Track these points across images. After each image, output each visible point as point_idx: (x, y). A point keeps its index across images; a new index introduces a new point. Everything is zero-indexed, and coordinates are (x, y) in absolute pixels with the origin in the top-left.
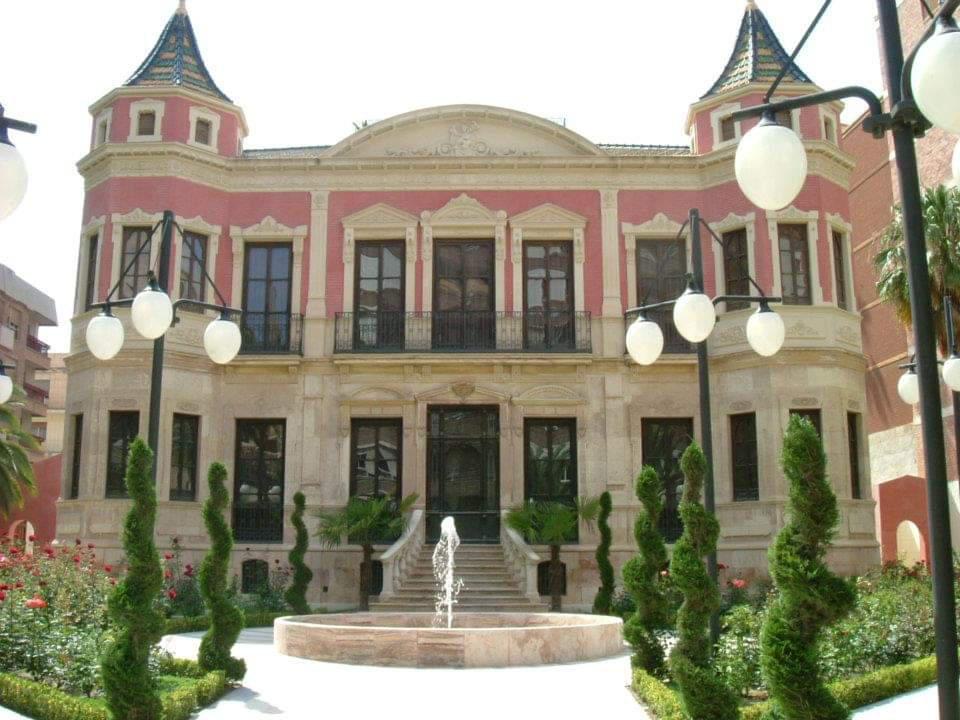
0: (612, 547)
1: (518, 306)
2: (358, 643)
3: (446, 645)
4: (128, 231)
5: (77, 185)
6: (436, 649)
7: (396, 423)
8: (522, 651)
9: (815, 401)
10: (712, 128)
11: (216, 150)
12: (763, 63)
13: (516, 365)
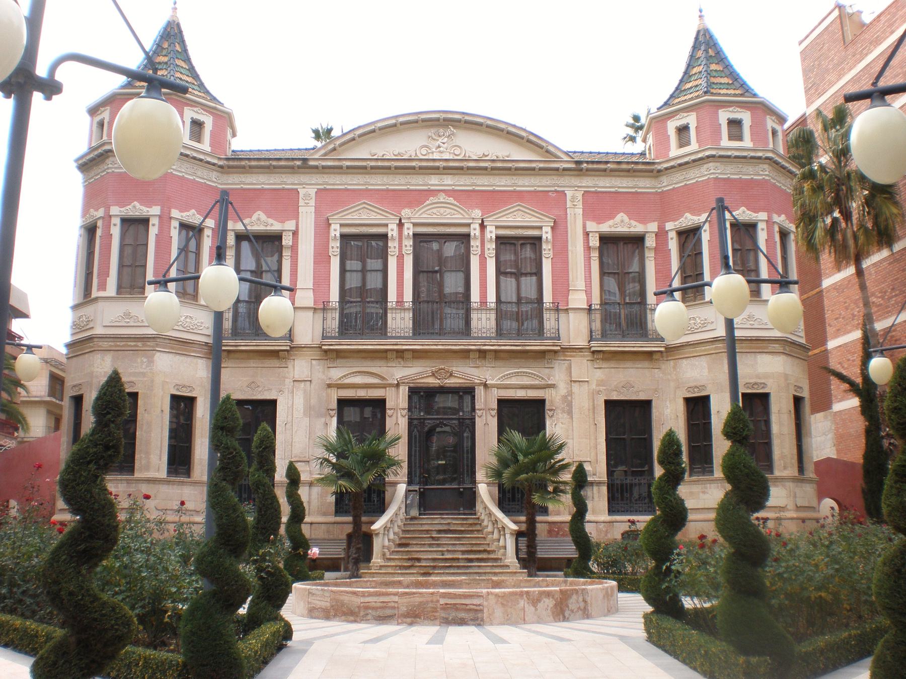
0: (588, 517)
1: (492, 297)
2: (381, 605)
3: (466, 605)
4: (127, 222)
5: (76, 182)
6: (457, 609)
7: (380, 404)
8: (536, 610)
9: (764, 385)
10: (669, 136)
11: (208, 149)
12: (714, 77)
13: (490, 351)
